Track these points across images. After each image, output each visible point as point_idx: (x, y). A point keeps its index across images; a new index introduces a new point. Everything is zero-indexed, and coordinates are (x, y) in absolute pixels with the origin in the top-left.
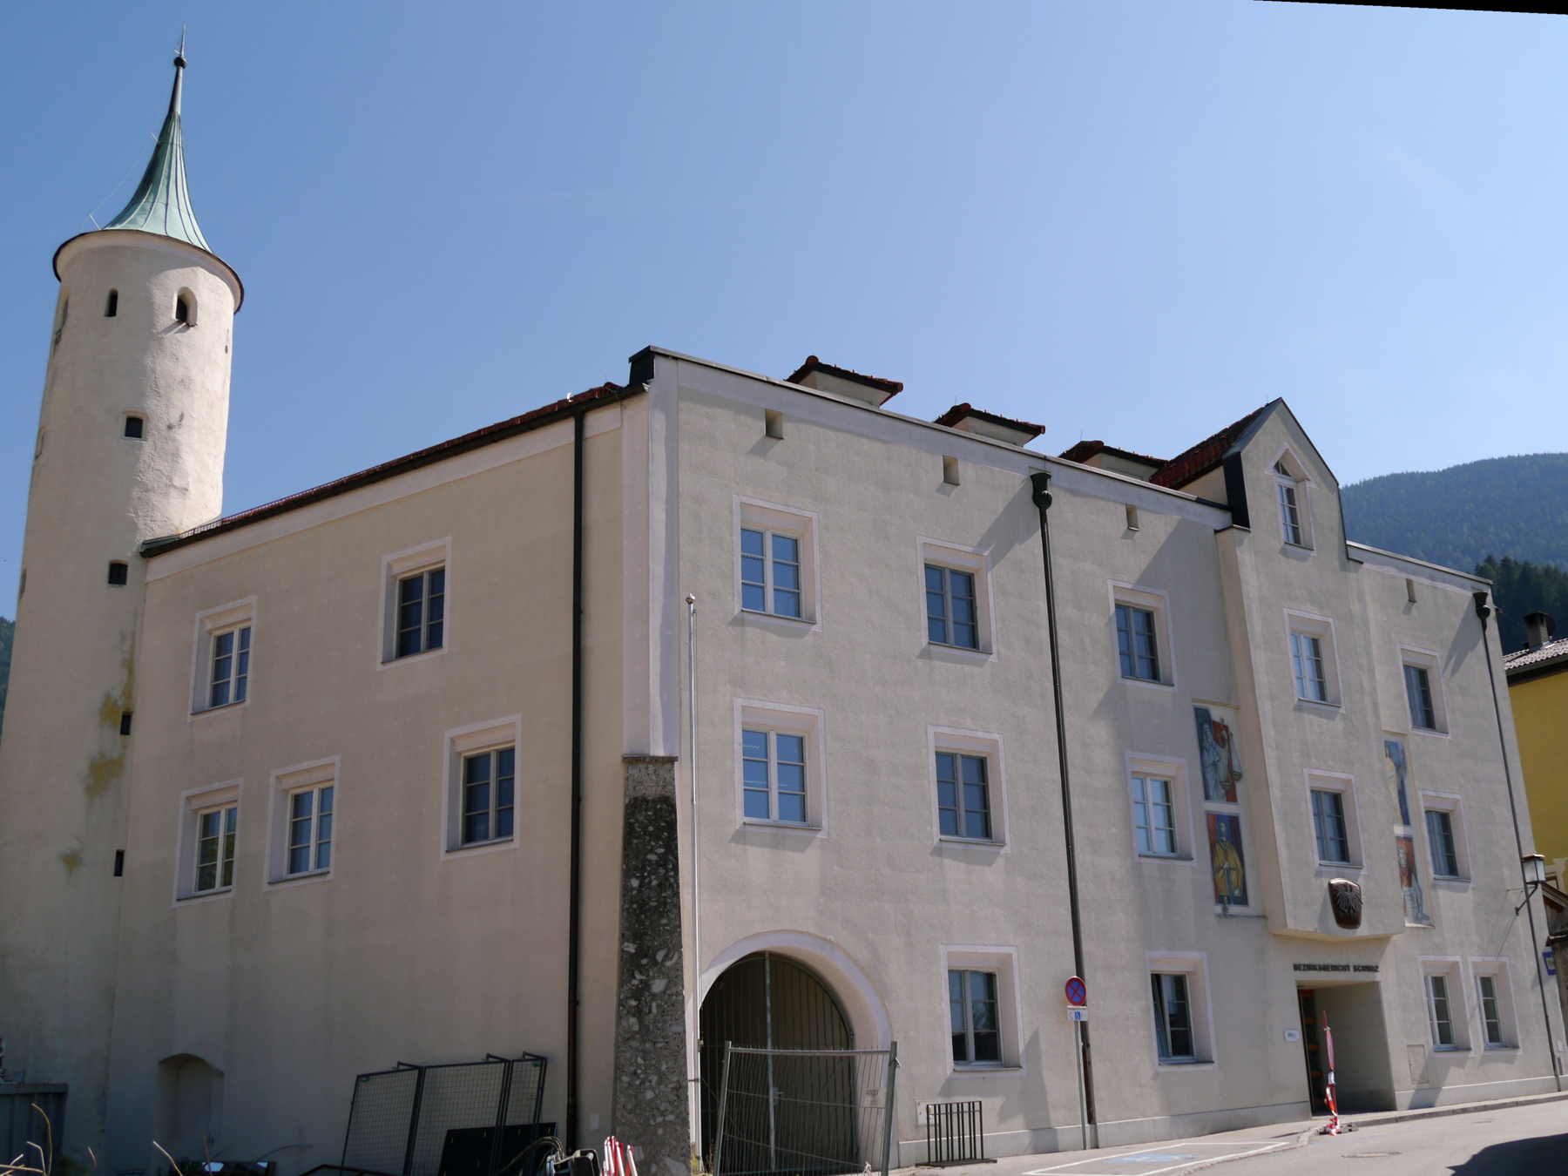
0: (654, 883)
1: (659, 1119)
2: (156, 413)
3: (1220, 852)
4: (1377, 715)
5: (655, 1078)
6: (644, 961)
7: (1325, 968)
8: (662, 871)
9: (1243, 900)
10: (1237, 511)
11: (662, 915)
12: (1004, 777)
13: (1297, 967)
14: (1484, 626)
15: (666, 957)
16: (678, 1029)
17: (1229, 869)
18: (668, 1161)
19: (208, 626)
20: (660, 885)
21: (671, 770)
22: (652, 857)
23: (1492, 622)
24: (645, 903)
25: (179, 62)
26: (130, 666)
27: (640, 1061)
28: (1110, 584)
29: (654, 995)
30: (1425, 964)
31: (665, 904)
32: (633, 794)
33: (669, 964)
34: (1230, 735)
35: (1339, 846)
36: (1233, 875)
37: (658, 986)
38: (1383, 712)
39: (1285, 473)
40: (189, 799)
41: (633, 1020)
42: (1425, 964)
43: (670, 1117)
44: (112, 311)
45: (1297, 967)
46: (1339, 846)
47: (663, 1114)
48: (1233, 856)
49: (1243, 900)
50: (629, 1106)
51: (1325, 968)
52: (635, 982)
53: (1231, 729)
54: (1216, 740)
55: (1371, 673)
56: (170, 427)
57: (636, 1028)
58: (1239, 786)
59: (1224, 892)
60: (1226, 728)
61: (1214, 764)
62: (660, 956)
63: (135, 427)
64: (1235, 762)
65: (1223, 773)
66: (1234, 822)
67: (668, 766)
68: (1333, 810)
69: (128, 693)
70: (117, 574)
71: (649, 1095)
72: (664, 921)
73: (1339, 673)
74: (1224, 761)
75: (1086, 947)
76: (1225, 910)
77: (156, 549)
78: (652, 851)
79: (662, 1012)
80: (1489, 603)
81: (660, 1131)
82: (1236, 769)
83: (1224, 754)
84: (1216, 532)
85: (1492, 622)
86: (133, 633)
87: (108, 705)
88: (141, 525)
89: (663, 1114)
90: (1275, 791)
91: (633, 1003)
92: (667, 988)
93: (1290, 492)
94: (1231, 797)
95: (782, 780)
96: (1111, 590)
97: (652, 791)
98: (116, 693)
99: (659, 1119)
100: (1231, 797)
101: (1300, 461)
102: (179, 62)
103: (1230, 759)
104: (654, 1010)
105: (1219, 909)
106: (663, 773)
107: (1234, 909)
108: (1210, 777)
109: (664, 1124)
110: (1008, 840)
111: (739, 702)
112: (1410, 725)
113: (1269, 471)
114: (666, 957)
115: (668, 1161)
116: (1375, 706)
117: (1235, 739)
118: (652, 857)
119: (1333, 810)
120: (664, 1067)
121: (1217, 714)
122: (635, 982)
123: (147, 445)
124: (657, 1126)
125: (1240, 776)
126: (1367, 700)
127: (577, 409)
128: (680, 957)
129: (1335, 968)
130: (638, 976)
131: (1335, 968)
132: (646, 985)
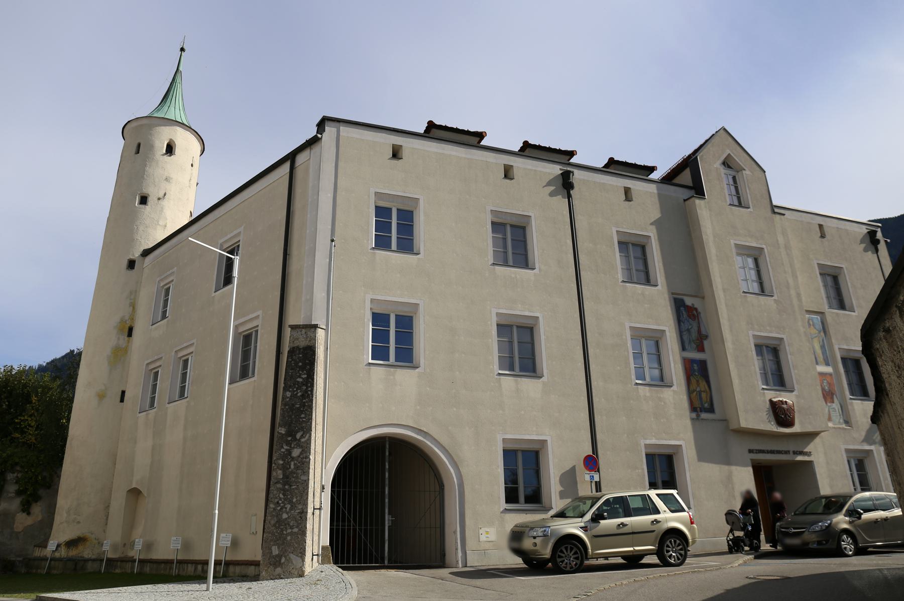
0: (299, 394)
1: (289, 531)
2: (153, 193)
3: (693, 380)
4: (800, 300)
5: (288, 506)
6: (289, 439)
7: (772, 452)
8: (304, 388)
9: (711, 410)
10: (698, 189)
11: (302, 412)
12: (543, 337)
13: (751, 451)
14: (877, 251)
15: (302, 436)
16: (303, 478)
17: (700, 392)
18: (292, 556)
19: (162, 284)
20: (302, 396)
21: (315, 332)
22: (300, 380)
23: (882, 247)
24: (293, 405)
25: (182, 50)
26: (133, 306)
27: (281, 496)
28: (614, 230)
29: (293, 459)
30: (847, 451)
31: (304, 406)
32: (292, 345)
33: (303, 440)
34: (699, 313)
35: (778, 377)
36: (704, 395)
37: (296, 452)
38: (803, 298)
39: (729, 167)
40: (148, 364)
41: (280, 472)
42: (847, 451)
43: (296, 530)
44: (138, 152)
45: (751, 451)
46: (778, 377)
47: (292, 528)
48: (703, 384)
49: (711, 410)
50: (273, 522)
51: (772, 452)
52: (283, 450)
53: (700, 310)
54: (689, 316)
55: (795, 276)
56: (159, 199)
57: (281, 477)
58: (705, 343)
59: (697, 404)
60: (696, 309)
61: (688, 330)
62: (298, 436)
63: (144, 200)
64: (703, 329)
65: (694, 335)
66: (703, 364)
67: (313, 330)
68: (772, 354)
69: (132, 319)
70: (131, 264)
71: (285, 516)
72: (303, 416)
73: (772, 276)
74: (695, 328)
75: (599, 436)
76: (698, 416)
77: (146, 253)
78: (300, 377)
79: (297, 468)
80: (879, 235)
81: (289, 538)
82: (703, 332)
83: (695, 324)
84: (685, 200)
85: (882, 247)
86: (136, 291)
87: (122, 321)
88: (143, 241)
89: (292, 528)
90: (729, 345)
91: (281, 462)
92: (301, 453)
93: (734, 178)
94: (701, 349)
95: (394, 337)
96: (615, 233)
97: (302, 343)
98: (127, 318)
99: (289, 531)
100: (701, 349)
101: (739, 159)
102: (182, 50)
103: (699, 327)
104: (292, 467)
105: (694, 415)
106: (310, 334)
107: (704, 415)
108: (685, 337)
109: (291, 534)
110: (545, 374)
111: (369, 297)
112: (827, 307)
113: (718, 164)
114: (302, 436)
115: (292, 556)
116: (799, 295)
117: (702, 315)
118: (300, 380)
119: (772, 354)
120: (294, 500)
121: (689, 301)
122: (283, 450)
123: (147, 209)
124: (287, 535)
125: (706, 337)
126: (793, 292)
127: (291, 157)
128: (310, 436)
129: (779, 452)
130: (285, 447)
131: (779, 452)
132: (289, 452)
